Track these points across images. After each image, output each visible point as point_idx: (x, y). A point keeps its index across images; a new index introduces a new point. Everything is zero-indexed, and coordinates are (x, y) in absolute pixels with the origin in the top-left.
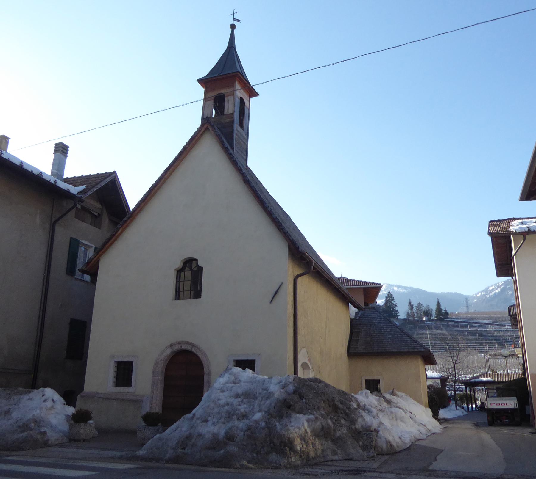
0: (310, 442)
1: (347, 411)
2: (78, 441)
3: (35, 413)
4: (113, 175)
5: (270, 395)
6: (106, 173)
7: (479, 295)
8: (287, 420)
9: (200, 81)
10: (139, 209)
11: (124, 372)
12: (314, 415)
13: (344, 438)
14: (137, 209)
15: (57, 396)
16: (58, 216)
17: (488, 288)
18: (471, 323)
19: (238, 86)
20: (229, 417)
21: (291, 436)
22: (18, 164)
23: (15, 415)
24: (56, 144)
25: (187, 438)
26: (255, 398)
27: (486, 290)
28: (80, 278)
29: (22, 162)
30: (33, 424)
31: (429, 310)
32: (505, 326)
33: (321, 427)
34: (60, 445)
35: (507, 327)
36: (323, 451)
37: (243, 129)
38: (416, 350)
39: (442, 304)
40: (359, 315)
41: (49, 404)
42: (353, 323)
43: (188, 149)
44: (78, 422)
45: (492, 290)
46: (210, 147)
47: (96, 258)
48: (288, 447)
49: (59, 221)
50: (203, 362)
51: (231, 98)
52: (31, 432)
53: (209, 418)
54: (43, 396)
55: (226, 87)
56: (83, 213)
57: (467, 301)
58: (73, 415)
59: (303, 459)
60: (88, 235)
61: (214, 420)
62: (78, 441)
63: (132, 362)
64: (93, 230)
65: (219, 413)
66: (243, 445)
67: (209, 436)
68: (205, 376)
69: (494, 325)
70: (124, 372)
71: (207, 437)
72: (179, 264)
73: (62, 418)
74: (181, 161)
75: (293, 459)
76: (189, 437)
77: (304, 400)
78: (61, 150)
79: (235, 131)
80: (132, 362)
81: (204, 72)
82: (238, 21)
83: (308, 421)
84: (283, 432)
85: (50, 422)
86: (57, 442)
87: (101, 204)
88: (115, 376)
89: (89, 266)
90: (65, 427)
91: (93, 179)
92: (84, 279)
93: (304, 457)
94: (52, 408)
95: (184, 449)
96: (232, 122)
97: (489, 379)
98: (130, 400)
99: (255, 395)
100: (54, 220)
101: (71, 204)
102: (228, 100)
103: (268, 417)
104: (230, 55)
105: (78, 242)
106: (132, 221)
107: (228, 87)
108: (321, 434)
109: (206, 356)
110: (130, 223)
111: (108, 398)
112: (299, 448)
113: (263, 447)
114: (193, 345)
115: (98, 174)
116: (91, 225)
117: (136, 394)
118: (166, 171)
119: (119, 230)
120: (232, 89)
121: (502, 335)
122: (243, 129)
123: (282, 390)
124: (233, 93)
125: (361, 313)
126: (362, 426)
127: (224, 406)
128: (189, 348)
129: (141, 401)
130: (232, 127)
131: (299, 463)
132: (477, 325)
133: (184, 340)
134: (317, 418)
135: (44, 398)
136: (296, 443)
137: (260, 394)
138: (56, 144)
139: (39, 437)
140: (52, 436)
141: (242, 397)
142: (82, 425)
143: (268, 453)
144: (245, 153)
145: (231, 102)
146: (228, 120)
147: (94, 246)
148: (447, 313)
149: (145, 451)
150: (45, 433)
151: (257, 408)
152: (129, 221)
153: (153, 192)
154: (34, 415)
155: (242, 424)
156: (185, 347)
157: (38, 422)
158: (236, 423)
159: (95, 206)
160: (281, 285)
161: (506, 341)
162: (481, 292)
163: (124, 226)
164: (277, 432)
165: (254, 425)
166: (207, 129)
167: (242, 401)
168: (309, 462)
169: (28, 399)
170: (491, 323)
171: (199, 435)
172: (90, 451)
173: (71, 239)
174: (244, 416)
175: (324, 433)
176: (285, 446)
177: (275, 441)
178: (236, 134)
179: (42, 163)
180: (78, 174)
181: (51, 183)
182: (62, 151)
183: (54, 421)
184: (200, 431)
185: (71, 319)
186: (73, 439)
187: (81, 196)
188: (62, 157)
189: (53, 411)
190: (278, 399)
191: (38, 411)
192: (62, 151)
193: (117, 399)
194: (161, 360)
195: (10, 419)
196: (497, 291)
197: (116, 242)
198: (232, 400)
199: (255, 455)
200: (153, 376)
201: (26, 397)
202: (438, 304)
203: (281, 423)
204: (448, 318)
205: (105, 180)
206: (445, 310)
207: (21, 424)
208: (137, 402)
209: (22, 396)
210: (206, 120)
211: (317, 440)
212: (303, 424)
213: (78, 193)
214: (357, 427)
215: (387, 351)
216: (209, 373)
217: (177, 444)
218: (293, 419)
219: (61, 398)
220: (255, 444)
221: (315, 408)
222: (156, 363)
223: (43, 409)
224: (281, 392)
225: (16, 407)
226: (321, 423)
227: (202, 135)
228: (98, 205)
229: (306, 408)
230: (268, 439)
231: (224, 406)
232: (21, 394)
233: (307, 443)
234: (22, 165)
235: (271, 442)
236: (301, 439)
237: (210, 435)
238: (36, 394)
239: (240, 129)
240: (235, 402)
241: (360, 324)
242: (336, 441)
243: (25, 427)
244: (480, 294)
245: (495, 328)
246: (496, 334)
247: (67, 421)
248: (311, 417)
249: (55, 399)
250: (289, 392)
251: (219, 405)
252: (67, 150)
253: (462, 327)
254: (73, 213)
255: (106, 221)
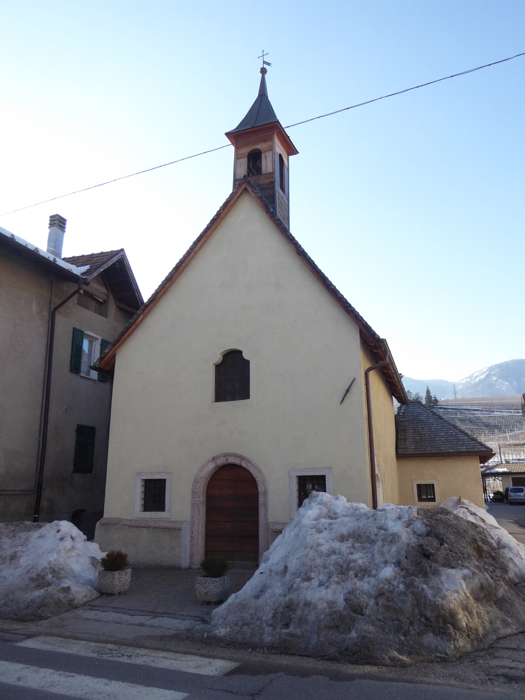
0: (474, 611)
1: (494, 554)
2: (112, 595)
3: (51, 559)
4: (121, 253)
5: (394, 538)
6: (112, 251)
7: (464, 382)
8: (437, 580)
9: (227, 134)
10: (163, 290)
11: (154, 493)
12: (468, 568)
13: (510, 599)
14: (161, 290)
15: (75, 531)
16: (59, 302)
17: (473, 375)
18: (460, 409)
19: (277, 142)
20: (342, 573)
21: (452, 606)
22: (9, 236)
23: (24, 561)
24: (51, 217)
25: (288, 607)
26: (373, 542)
27: (471, 377)
28: (86, 376)
29: (12, 235)
30: (50, 576)
31: (419, 397)
32: (494, 411)
33: (479, 585)
34: (88, 605)
35: (496, 413)
36: (491, 622)
37: (284, 193)
38: (476, 450)
39: (431, 392)
40: (402, 411)
41: (68, 543)
42: (397, 418)
43: (222, 215)
44: (110, 570)
45: (477, 377)
46: (249, 211)
47: (111, 352)
48: (450, 623)
49: (59, 309)
50: (257, 479)
51: (269, 154)
52: (50, 589)
53: (313, 575)
54: (58, 531)
55: (260, 145)
56: (87, 299)
57: (454, 388)
58: (103, 560)
59: (472, 640)
60: (96, 327)
61: (321, 577)
62: (112, 595)
63: (164, 480)
64: (97, 319)
65: (325, 567)
66: (380, 620)
67: (322, 605)
68: (260, 496)
69: (483, 411)
70: (154, 493)
71: (320, 607)
72: (218, 358)
73: (86, 561)
74: (214, 230)
75: (461, 643)
76: (290, 607)
77: (446, 545)
78: (58, 223)
79: (277, 195)
80: (164, 480)
81: (233, 125)
82: (269, 64)
83: (465, 578)
84: (439, 601)
85: (72, 570)
86: (85, 600)
87: (106, 288)
88: (143, 497)
89: (103, 362)
90: (91, 574)
91: (97, 258)
92: (91, 377)
93: (473, 637)
94: (73, 548)
95: (287, 625)
96: (273, 183)
97: (505, 470)
98: (165, 529)
99: (368, 537)
100: (53, 307)
101: (74, 287)
102: (266, 157)
103: (403, 573)
104: (262, 105)
105: (82, 332)
106: (155, 304)
107: (265, 141)
108: (482, 595)
109: (260, 472)
110: (152, 308)
111: (134, 526)
112: (464, 624)
113: (411, 623)
114: (242, 458)
115: (102, 253)
116: (95, 312)
117: (172, 520)
118: (196, 244)
119: (139, 316)
120: (270, 143)
121: (491, 421)
122: (284, 193)
123: (408, 530)
124: (271, 149)
125: (403, 407)
126: (516, 574)
127: (329, 555)
128: (237, 461)
129: (180, 529)
130: (274, 188)
131: (469, 647)
132: (467, 412)
133: (231, 452)
134: (474, 573)
135: (59, 535)
136: (460, 617)
137: (376, 535)
138: (51, 217)
139: (61, 596)
140: (80, 592)
141: (351, 540)
142: (117, 574)
143: (420, 634)
144: (287, 221)
145: (269, 159)
146: (267, 181)
147: (100, 338)
148: (436, 401)
149: (228, 629)
150: (68, 588)
151: (378, 559)
152: (152, 305)
153: (181, 268)
154: (49, 563)
155: (365, 585)
156: (232, 460)
157: (57, 572)
158: (359, 584)
159: (99, 290)
160: (353, 381)
161: (496, 426)
162: (466, 378)
163: (146, 311)
164: (430, 600)
165: (386, 587)
166: (245, 189)
167: (353, 546)
168: (486, 646)
169: (39, 537)
170: (480, 409)
171: (307, 604)
172: (138, 619)
173: (74, 329)
174: (364, 572)
175: (484, 594)
176: (445, 622)
177: (429, 614)
178: (279, 199)
179: (35, 237)
180: (78, 253)
181: (50, 260)
182: (60, 225)
183: (76, 567)
184: (308, 598)
185: (78, 425)
186: (104, 593)
187: (85, 277)
188: (59, 231)
189: (73, 553)
190: (409, 544)
191: (55, 556)
192: (60, 225)
193: (148, 527)
194: (201, 478)
195: (17, 568)
196: (482, 377)
197: (135, 332)
198: (337, 545)
199: (403, 638)
200: (192, 498)
201: (36, 534)
202: (428, 392)
203: (430, 585)
204: (438, 405)
205: (113, 259)
206: (435, 398)
207: (34, 575)
208: (174, 530)
209: (30, 533)
210: (237, 183)
211: (480, 607)
212: (461, 584)
213: (82, 274)
214: (510, 576)
215: (442, 451)
216: (265, 493)
217: (274, 616)
218: (444, 578)
219: (81, 533)
220: (398, 620)
221: (466, 555)
222: (196, 481)
223: (62, 551)
224: (407, 532)
225: (24, 549)
226: (479, 579)
227: (239, 197)
228: (103, 290)
229: (453, 557)
230: (417, 611)
231: (329, 555)
232: (29, 530)
233: (471, 613)
234: (13, 238)
235: (421, 614)
236: (463, 609)
237: (325, 604)
238: (49, 530)
239: (280, 191)
240: (344, 547)
241: (406, 421)
242: (501, 603)
243: (39, 581)
244: (465, 380)
245: (484, 414)
246: (485, 420)
247: (93, 565)
248: (466, 571)
249: (74, 536)
250: (418, 532)
251: (322, 553)
252: (65, 224)
253: (452, 414)
254: (76, 297)
255: (112, 308)
